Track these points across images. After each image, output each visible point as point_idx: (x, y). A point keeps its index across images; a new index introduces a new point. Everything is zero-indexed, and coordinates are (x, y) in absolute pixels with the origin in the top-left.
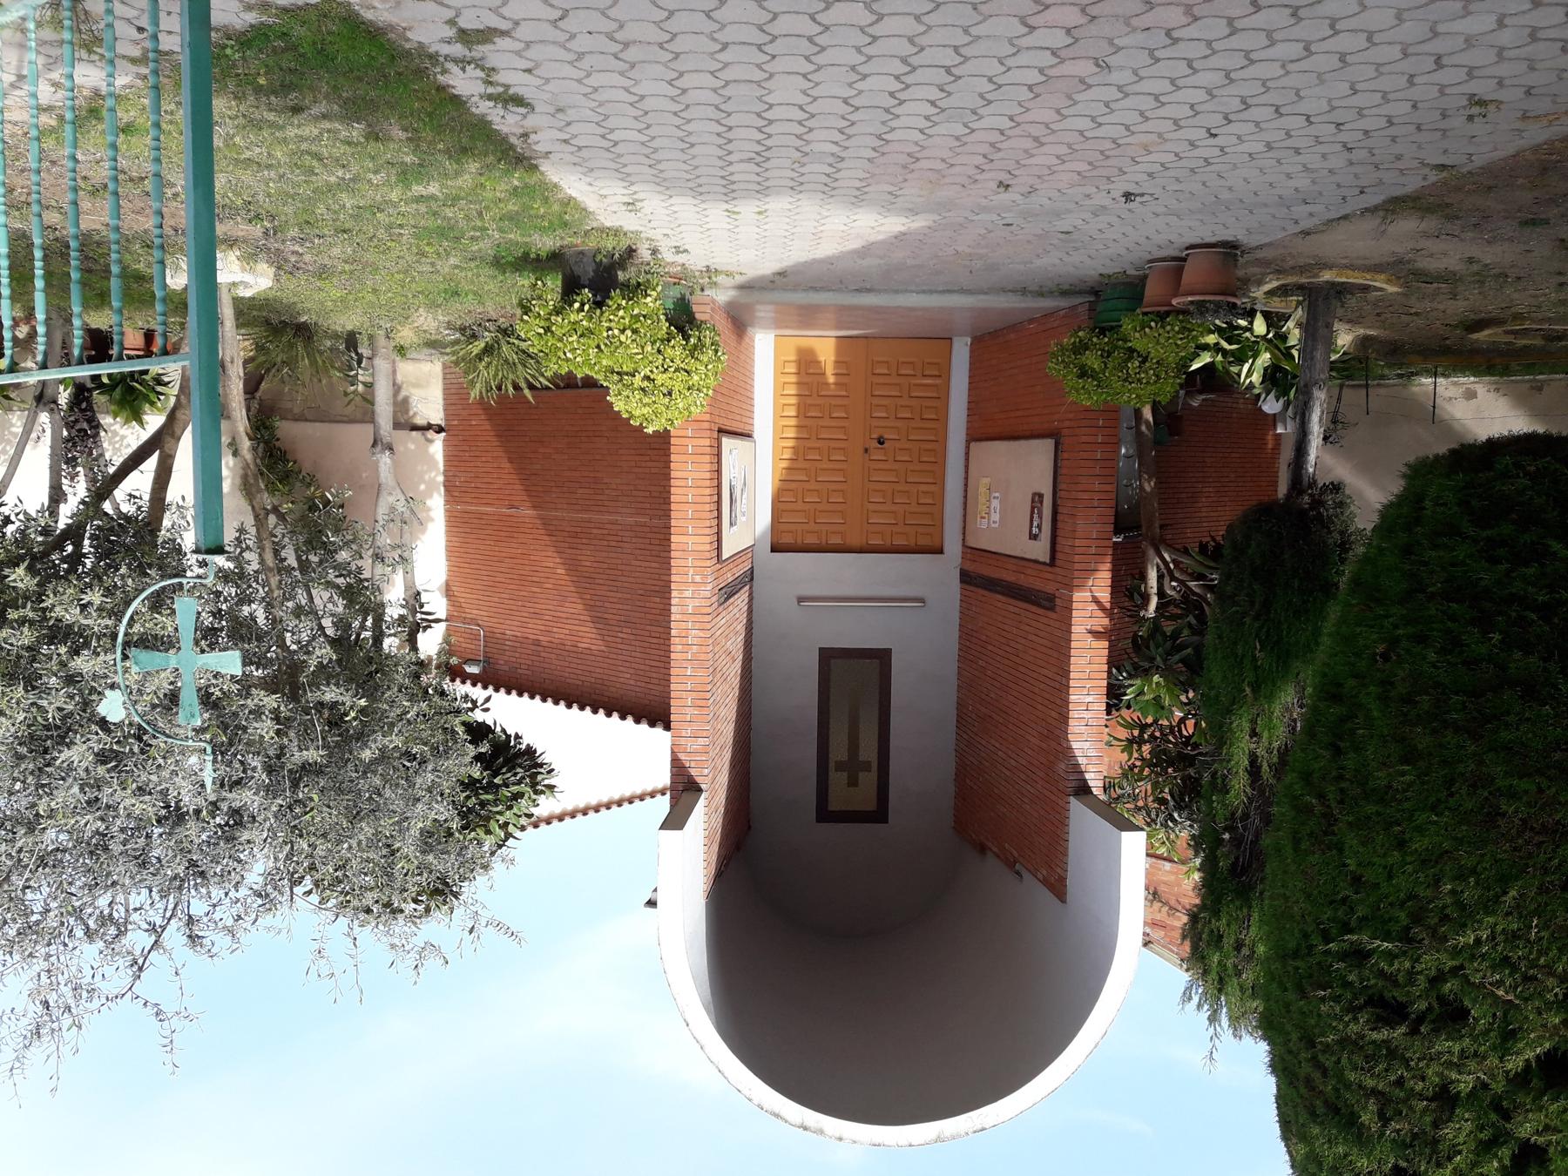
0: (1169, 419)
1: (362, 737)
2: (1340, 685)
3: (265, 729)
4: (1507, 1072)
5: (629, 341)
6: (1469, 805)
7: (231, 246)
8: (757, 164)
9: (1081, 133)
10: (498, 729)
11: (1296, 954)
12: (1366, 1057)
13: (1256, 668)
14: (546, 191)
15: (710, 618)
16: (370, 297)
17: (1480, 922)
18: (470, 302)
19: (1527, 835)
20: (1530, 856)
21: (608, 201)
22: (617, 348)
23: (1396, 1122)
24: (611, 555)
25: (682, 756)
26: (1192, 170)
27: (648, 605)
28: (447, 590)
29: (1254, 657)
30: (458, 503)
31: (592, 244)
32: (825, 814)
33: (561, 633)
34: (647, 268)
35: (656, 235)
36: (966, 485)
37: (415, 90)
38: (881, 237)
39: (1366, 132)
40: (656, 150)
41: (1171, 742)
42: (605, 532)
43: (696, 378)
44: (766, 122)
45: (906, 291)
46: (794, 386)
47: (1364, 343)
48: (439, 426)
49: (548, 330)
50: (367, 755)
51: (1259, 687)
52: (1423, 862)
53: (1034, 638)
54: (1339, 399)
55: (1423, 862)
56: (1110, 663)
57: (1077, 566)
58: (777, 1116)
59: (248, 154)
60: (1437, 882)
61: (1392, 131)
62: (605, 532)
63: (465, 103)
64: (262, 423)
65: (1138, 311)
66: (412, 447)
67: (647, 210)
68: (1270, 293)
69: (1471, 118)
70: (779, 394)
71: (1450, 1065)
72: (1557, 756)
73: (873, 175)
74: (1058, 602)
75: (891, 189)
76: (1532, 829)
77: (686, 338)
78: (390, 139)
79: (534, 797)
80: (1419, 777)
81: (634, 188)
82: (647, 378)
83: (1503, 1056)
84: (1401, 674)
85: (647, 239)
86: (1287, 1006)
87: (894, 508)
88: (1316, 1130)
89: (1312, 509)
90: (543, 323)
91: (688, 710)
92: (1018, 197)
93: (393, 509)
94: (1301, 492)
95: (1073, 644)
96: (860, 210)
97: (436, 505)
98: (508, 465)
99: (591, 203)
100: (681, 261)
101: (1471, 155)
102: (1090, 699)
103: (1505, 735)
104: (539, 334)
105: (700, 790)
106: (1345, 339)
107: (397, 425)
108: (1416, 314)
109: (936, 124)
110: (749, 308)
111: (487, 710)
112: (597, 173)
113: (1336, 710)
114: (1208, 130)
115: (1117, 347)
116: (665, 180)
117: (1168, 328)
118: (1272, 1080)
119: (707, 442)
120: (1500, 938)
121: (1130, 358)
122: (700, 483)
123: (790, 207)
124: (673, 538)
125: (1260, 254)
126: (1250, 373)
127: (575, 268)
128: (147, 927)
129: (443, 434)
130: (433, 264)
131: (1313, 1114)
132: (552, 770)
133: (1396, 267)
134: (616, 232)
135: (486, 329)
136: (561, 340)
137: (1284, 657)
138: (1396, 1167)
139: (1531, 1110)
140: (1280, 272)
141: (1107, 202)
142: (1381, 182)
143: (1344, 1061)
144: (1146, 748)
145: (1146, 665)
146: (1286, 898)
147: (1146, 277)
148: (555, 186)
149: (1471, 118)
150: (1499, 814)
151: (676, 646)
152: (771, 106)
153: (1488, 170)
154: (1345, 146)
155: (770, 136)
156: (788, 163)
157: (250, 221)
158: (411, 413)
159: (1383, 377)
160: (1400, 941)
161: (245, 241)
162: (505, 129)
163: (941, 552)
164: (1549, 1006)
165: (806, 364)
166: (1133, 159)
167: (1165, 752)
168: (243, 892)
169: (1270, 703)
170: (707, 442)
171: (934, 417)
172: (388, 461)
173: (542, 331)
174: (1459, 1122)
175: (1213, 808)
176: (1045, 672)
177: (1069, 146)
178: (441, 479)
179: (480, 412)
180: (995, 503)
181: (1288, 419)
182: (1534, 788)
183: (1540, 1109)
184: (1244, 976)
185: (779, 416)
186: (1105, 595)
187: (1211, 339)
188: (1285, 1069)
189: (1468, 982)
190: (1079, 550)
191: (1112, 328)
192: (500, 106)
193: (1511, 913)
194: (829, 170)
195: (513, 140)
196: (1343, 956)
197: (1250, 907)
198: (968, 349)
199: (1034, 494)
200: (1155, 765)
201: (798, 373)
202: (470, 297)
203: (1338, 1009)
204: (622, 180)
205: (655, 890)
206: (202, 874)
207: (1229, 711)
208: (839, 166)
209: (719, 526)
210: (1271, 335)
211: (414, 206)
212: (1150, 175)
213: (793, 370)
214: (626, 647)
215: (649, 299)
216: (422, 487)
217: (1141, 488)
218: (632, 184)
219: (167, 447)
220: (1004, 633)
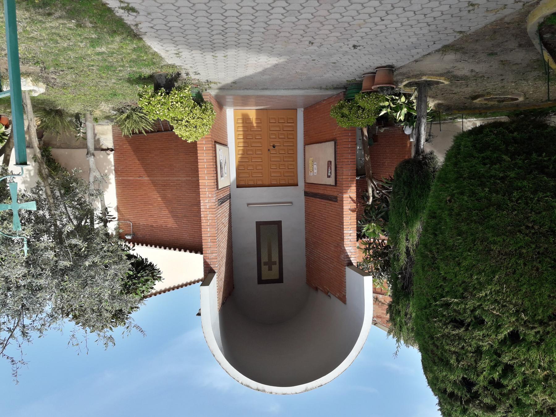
0: (373, 137)
1: (86, 257)
2: (435, 213)
3: (50, 255)
4: (498, 340)
5: (179, 106)
6: (481, 248)
7: (28, 76)
8: (223, 35)
9: (337, 20)
10: (139, 257)
11: (425, 308)
12: (451, 340)
13: (407, 217)
14: (146, 49)
15: (215, 210)
16: (83, 97)
17: (486, 288)
18: (120, 99)
19: (501, 256)
20: (502, 263)
21: (169, 53)
22: (175, 109)
23: (463, 362)
24: (178, 192)
25: (208, 261)
26: (376, 35)
27: (192, 209)
28: (118, 209)
29: (406, 213)
30: (120, 177)
31: (164, 71)
32: (261, 281)
33: (161, 222)
34: (185, 81)
35: (187, 67)
36: (305, 161)
37: (94, 5)
38: (269, 66)
39: (434, 18)
40: (185, 30)
41: (379, 249)
42: (175, 184)
43: (205, 121)
44: (224, 18)
45: (280, 89)
46: (241, 128)
47: (438, 106)
48: (112, 149)
49: (149, 103)
50: (87, 264)
51: (408, 223)
52: (467, 270)
53: (331, 212)
54: (431, 129)
55: (467, 270)
56: (357, 219)
57: (344, 185)
58: (248, 386)
59: (32, 35)
60: (472, 275)
61: (443, 17)
62: (175, 184)
63: (113, 11)
64: (45, 148)
65: (361, 92)
66: (102, 157)
67: (183, 57)
68: (405, 86)
69: (469, 11)
70: (236, 131)
71: (479, 340)
72: (509, 228)
73: (265, 39)
74: (338, 199)
75: (271, 45)
76: (502, 254)
77: (201, 106)
78: (86, 27)
79: (153, 281)
80: (463, 240)
81: (178, 47)
82: (187, 121)
83: (497, 334)
84: (456, 206)
85: (185, 69)
86: (423, 326)
87: (280, 170)
88: (436, 368)
89: (423, 160)
90: (147, 101)
91: (209, 244)
92: (316, 48)
93: (95, 177)
94: (419, 155)
95: (344, 213)
96: (261, 55)
97: (112, 178)
98: (138, 162)
99: (163, 54)
100: (197, 78)
101: (470, 27)
102: (351, 232)
103: (491, 223)
104: (146, 105)
105: (215, 272)
106: (432, 104)
107: (96, 149)
108: (455, 93)
109: (286, 17)
110: (223, 97)
111: (134, 250)
112: (165, 41)
113: (434, 221)
114: (381, 18)
115: (354, 106)
116: (189, 43)
117: (371, 97)
118: (420, 354)
119: (211, 145)
120: (493, 293)
121: (359, 110)
122: (208, 149)
123: (235, 53)
124: (200, 181)
125: (401, 71)
126: (400, 116)
127: (159, 81)
128: (8, 330)
129: (113, 152)
130: (106, 83)
131: (434, 363)
132: (160, 271)
133: (447, 74)
134: (173, 66)
135: (127, 109)
136: (154, 106)
137: (416, 212)
138: (463, 378)
139: (507, 352)
140: (408, 77)
141: (348, 49)
142: (440, 39)
143: (444, 342)
144: (371, 251)
145: (370, 219)
146: (421, 288)
147: (362, 81)
148: (149, 47)
149: (469, 11)
150: (491, 250)
151: (203, 221)
152: (226, 10)
153: (476, 33)
154: (427, 24)
155: (226, 23)
156: (233, 35)
157: (35, 64)
158: (101, 144)
159: (445, 120)
160: (460, 298)
161: (33, 73)
162: (129, 22)
163: (297, 185)
164: (511, 315)
165: (245, 119)
166: (355, 31)
167: (377, 252)
168: (44, 315)
169: (412, 228)
170: (211, 145)
171: (292, 137)
172: (93, 159)
173: (147, 104)
174: (484, 360)
175: (395, 267)
176: (335, 224)
177: (333, 26)
178: (113, 168)
179: (126, 143)
180: (315, 166)
181: (414, 135)
182: (502, 240)
183: (510, 352)
184: (409, 325)
185: (237, 138)
186: (354, 196)
187: (387, 103)
188: (424, 349)
189: (484, 310)
190: (344, 180)
191: (352, 99)
192: (126, 12)
193: (496, 284)
194: (249, 37)
195: (133, 28)
196: (442, 306)
197: (409, 300)
198: (303, 113)
199: (328, 162)
200: (375, 257)
201: (243, 123)
202: (120, 96)
203: (441, 324)
204: (174, 43)
205: (200, 309)
206: (28, 309)
207: (398, 232)
208: (252, 35)
209: (217, 176)
210: (406, 102)
211: (97, 57)
212: (362, 37)
213: (241, 122)
214: (185, 226)
215: (186, 90)
216: (106, 171)
217: (365, 159)
218: (178, 45)
219: (8, 151)
220: (321, 212)
